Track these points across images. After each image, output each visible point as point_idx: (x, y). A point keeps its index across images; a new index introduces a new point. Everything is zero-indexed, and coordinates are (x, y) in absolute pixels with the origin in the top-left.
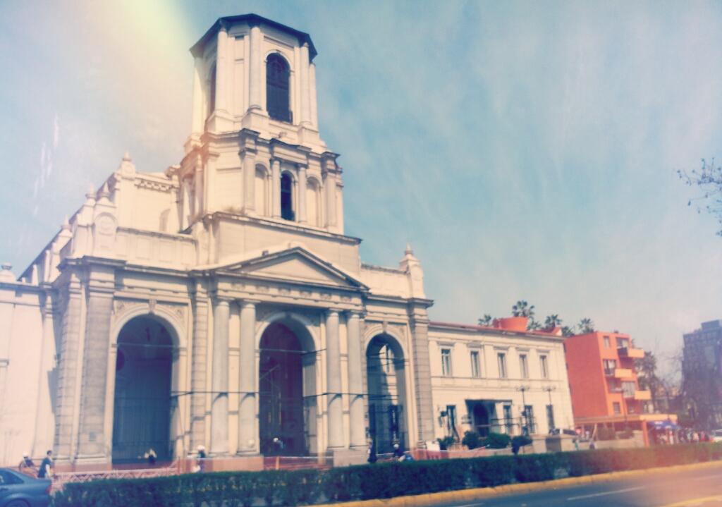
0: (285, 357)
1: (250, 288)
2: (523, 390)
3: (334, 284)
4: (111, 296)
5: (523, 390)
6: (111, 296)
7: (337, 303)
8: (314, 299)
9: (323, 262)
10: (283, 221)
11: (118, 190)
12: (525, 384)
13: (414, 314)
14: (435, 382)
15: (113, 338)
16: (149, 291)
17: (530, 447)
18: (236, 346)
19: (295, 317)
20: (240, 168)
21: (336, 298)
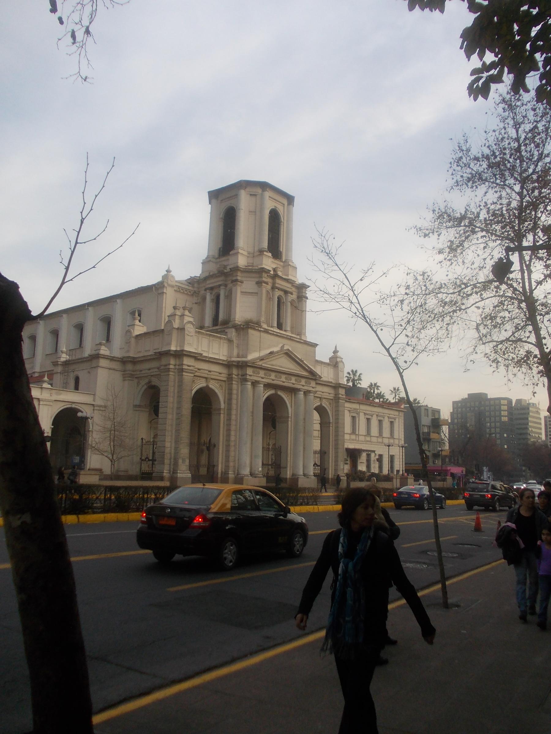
0: (273, 413)
1: (262, 373)
2: (389, 446)
3: (305, 373)
4: (193, 375)
5: (389, 446)
6: (193, 375)
7: (303, 386)
8: (292, 382)
9: (298, 358)
10: (278, 331)
11: (475, 100)
12: (392, 441)
13: (339, 394)
14: (347, 437)
15: (193, 392)
16: (207, 372)
17: (41, 331)
18: (360, 439)
19: (280, 393)
20: (257, 293)
21: (303, 381)
